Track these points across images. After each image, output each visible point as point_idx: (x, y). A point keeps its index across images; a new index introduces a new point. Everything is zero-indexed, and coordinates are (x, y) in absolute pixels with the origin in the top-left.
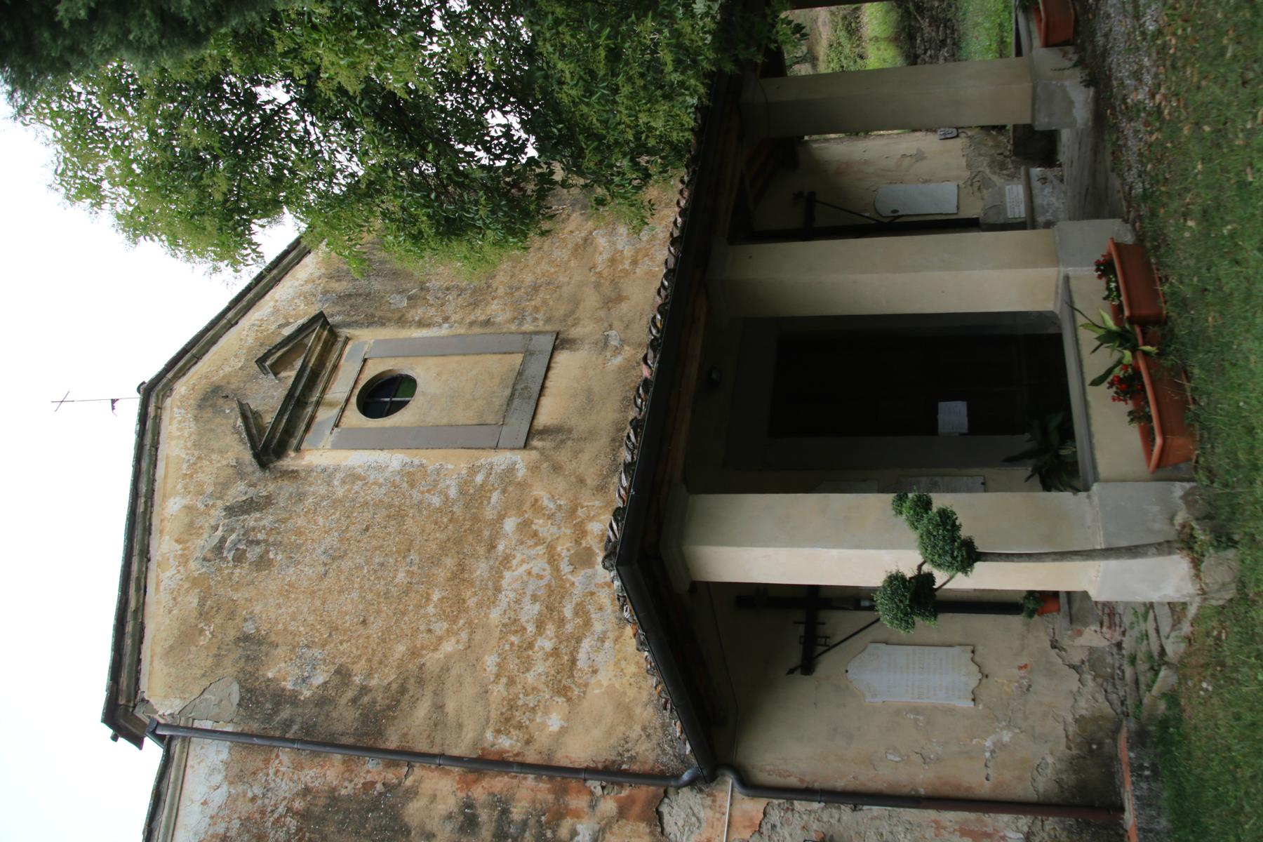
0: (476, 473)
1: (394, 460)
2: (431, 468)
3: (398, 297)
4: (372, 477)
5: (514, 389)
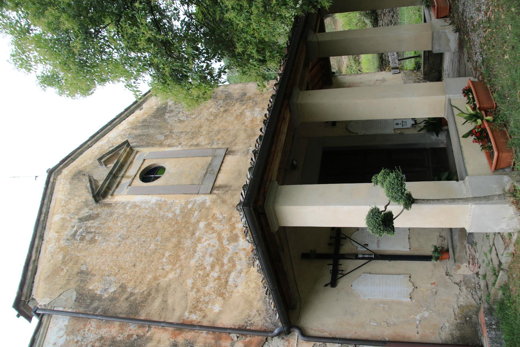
1: (153, 199)
2: (169, 202)
3: (160, 136)
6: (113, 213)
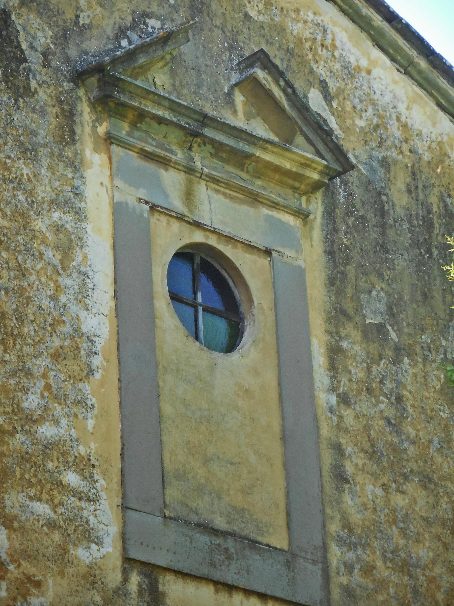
0: (81, 472)
1: (98, 322)
2: (87, 388)
3: (382, 307)
4: (69, 282)
5: (225, 534)
6: (35, 159)
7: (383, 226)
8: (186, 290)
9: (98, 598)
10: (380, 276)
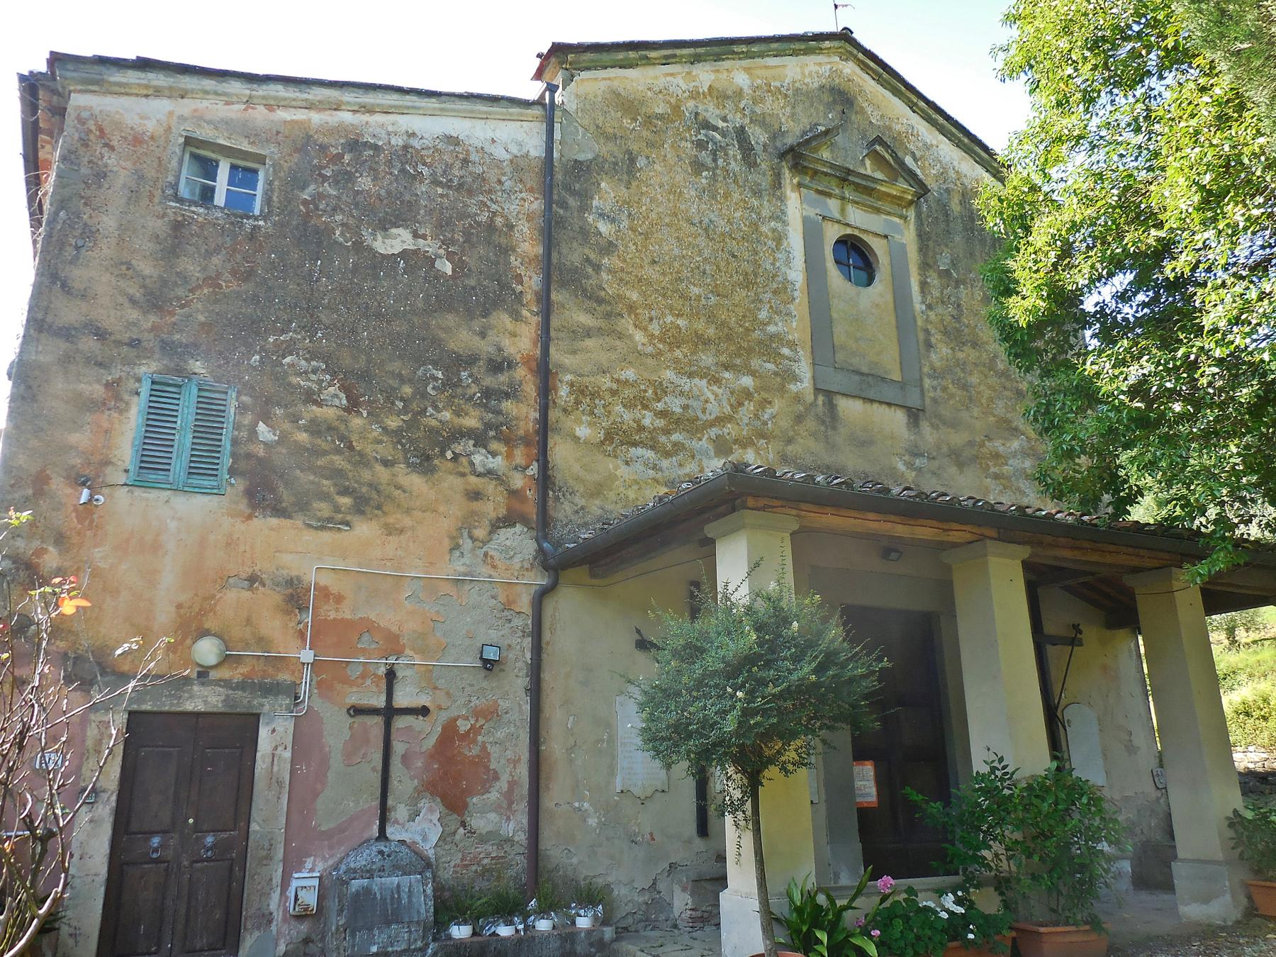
1: (796, 274)
2: (792, 307)
7: (947, 221)
8: (844, 258)
9: (801, 408)
10: (947, 246)
